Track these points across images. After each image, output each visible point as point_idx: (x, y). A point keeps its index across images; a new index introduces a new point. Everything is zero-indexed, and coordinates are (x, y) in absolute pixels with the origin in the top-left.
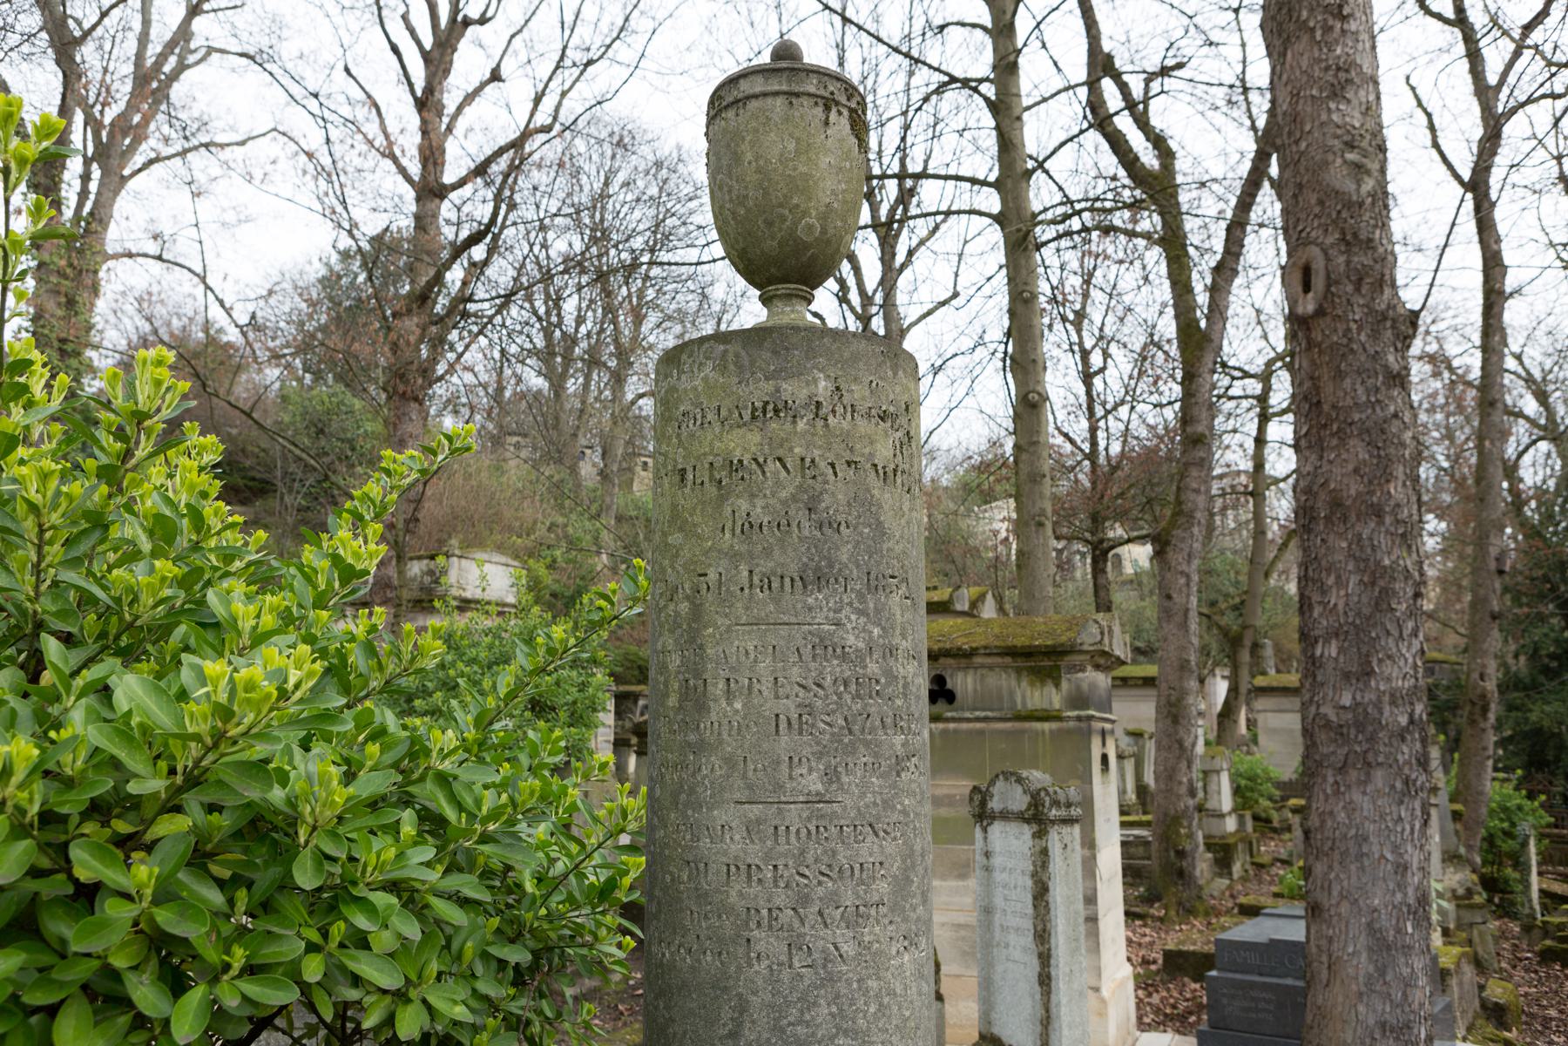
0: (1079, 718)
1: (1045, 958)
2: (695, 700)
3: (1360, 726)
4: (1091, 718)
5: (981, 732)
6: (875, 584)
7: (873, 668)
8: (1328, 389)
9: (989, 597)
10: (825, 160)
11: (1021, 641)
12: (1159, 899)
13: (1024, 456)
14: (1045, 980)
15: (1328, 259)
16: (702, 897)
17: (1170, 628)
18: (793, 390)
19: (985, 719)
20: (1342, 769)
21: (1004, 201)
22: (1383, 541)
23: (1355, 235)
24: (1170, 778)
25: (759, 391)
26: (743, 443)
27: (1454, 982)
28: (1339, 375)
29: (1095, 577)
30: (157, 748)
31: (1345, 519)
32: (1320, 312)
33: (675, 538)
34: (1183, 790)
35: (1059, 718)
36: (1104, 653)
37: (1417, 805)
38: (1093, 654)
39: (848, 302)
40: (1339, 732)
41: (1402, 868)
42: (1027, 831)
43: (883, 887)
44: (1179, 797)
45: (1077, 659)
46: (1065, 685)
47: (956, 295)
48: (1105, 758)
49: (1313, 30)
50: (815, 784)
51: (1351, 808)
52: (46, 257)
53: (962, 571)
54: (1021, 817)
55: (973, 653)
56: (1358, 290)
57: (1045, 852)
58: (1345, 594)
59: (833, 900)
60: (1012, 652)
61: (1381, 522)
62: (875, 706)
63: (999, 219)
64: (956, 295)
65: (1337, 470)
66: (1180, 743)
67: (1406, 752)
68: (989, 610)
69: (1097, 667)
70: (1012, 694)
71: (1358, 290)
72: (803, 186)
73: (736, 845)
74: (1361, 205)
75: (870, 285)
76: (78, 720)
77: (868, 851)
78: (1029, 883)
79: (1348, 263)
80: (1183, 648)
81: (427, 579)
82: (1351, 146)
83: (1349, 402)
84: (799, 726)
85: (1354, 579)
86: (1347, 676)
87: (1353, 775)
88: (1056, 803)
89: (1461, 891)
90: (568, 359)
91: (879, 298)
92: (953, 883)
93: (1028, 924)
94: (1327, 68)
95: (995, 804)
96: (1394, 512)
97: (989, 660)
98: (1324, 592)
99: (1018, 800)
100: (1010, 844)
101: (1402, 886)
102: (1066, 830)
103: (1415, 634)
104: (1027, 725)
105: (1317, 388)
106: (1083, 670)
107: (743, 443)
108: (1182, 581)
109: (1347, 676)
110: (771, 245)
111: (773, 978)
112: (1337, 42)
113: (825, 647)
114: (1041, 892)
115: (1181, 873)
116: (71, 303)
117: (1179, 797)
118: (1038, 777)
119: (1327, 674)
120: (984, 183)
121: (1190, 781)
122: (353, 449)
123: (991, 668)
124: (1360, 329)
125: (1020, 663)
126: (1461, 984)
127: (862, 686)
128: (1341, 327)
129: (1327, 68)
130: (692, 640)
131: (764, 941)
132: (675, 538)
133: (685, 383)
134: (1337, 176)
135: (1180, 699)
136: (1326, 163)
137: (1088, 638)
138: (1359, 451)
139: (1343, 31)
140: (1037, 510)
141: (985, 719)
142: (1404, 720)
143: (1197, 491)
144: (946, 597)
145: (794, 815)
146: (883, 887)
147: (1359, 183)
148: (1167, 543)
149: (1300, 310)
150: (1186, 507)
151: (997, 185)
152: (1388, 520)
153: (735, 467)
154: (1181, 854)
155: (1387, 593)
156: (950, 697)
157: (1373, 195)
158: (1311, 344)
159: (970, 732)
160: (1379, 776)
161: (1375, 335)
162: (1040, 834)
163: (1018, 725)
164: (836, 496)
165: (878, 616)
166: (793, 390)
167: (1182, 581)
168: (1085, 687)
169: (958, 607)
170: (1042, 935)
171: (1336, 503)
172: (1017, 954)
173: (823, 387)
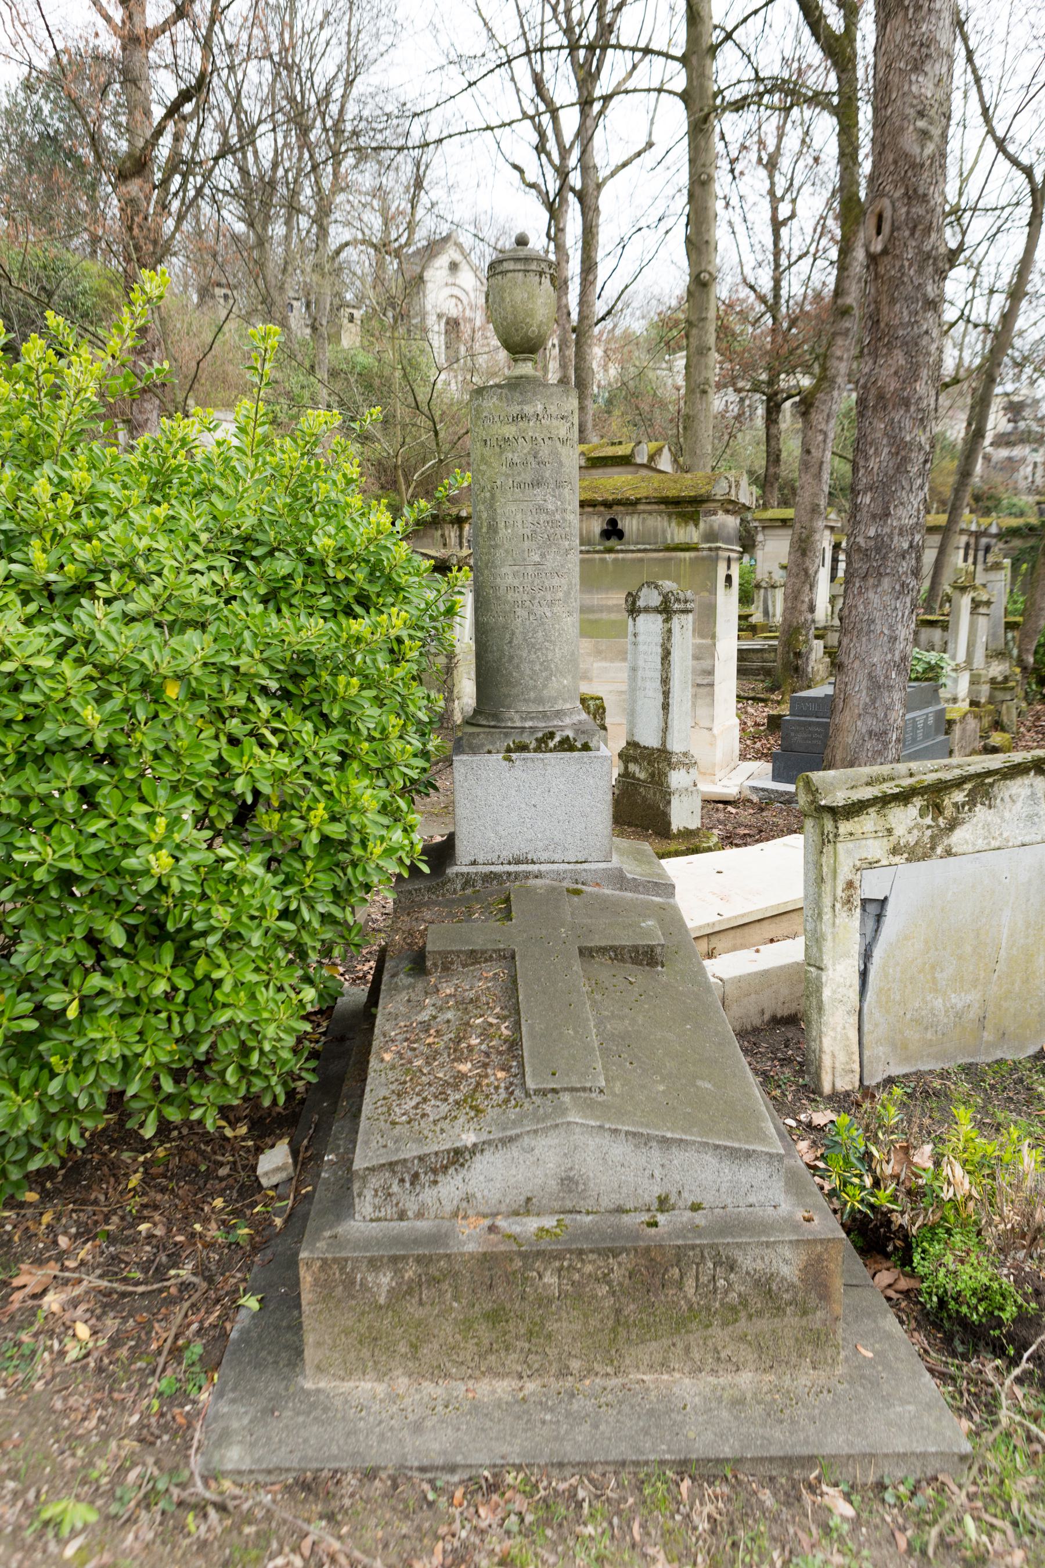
0: (710, 549)
1: (666, 694)
2: (493, 529)
3: (878, 550)
4: (718, 548)
5: (641, 560)
6: (559, 485)
7: (558, 517)
8: (885, 310)
9: (666, 450)
10: (540, 301)
11: (672, 493)
12: (778, 688)
13: (694, 331)
14: (666, 707)
15: (894, 210)
16: (498, 598)
17: (807, 478)
18: (528, 409)
19: (645, 551)
20: (864, 578)
21: (690, 79)
22: (908, 423)
23: (915, 190)
24: (796, 598)
25: (515, 410)
26: (509, 431)
27: (957, 729)
28: (893, 301)
29: (768, 428)
31: (885, 408)
32: (885, 252)
33: (483, 467)
34: (805, 607)
35: (696, 549)
36: (731, 502)
37: (908, 600)
38: (723, 503)
39: (548, 155)
40: (865, 554)
42: (660, 618)
43: (560, 595)
44: (801, 612)
45: (711, 506)
46: (702, 525)
47: (650, 145)
48: (729, 579)
49: (907, 8)
50: (537, 558)
51: (867, 603)
53: (649, 422)
54: (657, 610)
55: (638, 502)
56: (912, 234)
57: (670, 631)
58: (879, 460)
59: (544, 598)
60: (665, 501)
61: (907, 411)
62: (558, 531)
63: (685, 96)
64: (650, 145)
65: (884, 373)
67: (905, 566)
68: (665, 463)
69: (727, 512)
70: (664, 532)
71: (912, 234)
72: (530, 313)
73: (510, 580)
74: (922, 165)
75: (568, 136)
77: (556, 581)
78: (660, 650)
79: (908, 213)
80: (815, 495)
82: (921, 114)
83: (897, 322)
84: (532, 537)
85: (886, 450)
86: (874, 517)
87: (871, 581)
88: (678, 600)
89: (1000, 679)
90: (266, 204)
91: (576, 153)
93: (657, 675)
94: (914, 44)
95: (641, 603)
96: (917, 403)
97: (648, 507)
98: (867, 460)
99: (656, 600)
100: (650, 626)
101: (892, 650)
102: (683, 617)
103: (921, 487)
104: (674, 554)
105: (878, 310)
106: (715, 514)
107: (509, 431)
109: (874, 517)
110: (517, 339)
111: (523, 623)
112: (923, 19)
113: (540, 509)
114: (666, 655)
115: (797, 669)
117: (801, 612)
118: (668, 585)
119: (864, 515)
120: (673, 58)
122: (75, 308)
123: (650, 513)
124: (911, 266)
125: (671, 509)
126: (964, 730)
127: (553, 523)
128: (898, 264)
129: (914, 44)
130: (491, 507)
131: (520, 611)
132: (483, 467)
133: (485, 404)
134: (909, 142)
135: (808, 537)
136: (902, 129)
137: (720, 490)
138: (899, 358)
139: (930, 10)
140: (702, 379)
141: (645, 551)
142: (906, 546)
143: (840, 359)
144: (628, 452)
145: (530, 570)
146: (560, 595)
147: (922, 147)
148: (811, 405)
149: (872, 249)
150: (830, 373)
151: (684, 60)
152: (913, 409)
153: (506, 440)
154: (798, 655)
155: (905, 460)
156: (620, 535)
157: (932, 158)
158: (877, 276)
159: (633, 560)
160: (886, 582)
161: (921, 271)
162: (667, 620)
163: (667, 554)
164: (544, 452)
165: (560, 497)
166: (528, 409)
167: (821, 438)
168: (716, 526)
169: (639, 460)
170: (665, 681)
171: (881, 397)
172: (650, 693)
173: (539, 408)
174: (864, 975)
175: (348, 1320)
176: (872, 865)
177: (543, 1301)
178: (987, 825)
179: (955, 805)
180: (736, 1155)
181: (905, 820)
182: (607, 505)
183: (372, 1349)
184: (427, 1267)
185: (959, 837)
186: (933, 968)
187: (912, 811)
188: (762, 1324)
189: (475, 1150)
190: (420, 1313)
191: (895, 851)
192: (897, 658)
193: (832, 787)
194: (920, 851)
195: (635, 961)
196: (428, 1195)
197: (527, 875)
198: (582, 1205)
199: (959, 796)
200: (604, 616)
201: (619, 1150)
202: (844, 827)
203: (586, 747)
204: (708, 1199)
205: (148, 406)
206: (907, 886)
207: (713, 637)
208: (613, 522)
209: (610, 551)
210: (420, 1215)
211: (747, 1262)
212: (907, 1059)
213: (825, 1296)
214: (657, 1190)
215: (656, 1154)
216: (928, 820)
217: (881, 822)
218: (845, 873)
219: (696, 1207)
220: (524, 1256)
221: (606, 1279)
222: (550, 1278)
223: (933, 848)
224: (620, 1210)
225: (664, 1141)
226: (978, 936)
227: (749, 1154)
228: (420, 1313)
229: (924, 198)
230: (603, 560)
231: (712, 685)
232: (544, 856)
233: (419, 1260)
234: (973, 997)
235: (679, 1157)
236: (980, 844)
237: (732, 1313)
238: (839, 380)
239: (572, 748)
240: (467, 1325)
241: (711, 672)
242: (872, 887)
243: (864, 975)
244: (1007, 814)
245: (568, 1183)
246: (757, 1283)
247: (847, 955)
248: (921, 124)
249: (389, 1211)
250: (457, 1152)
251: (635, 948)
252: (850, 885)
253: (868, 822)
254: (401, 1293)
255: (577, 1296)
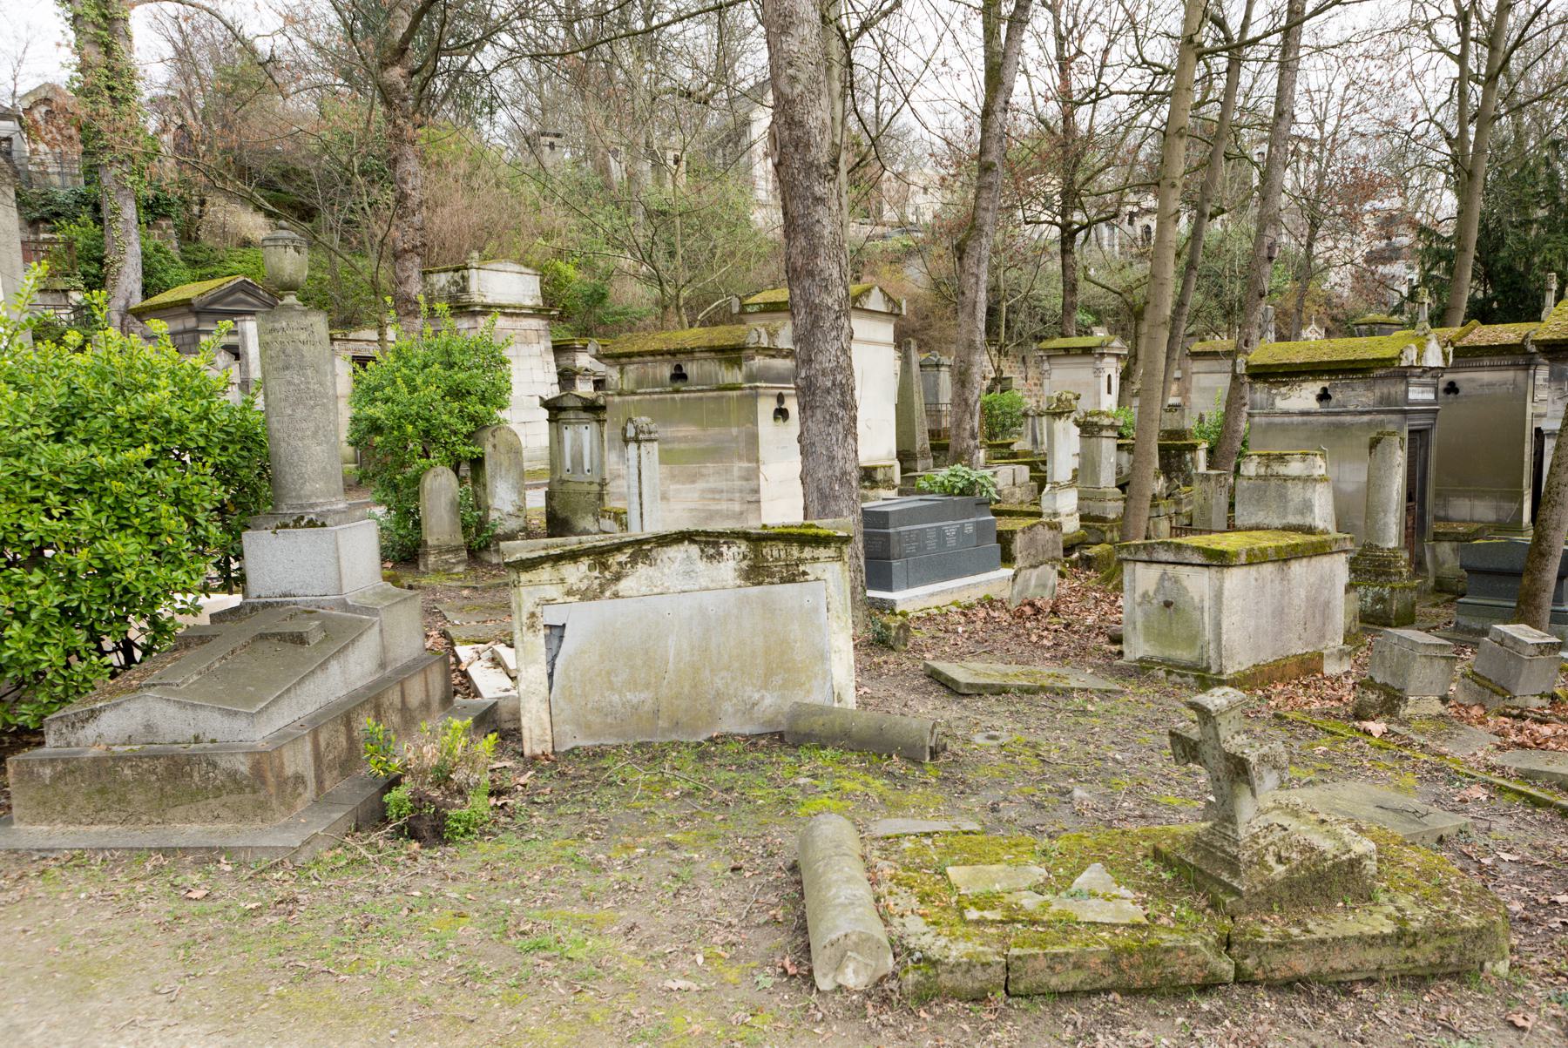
5: (701, 399)
6: (302, 368)
18: (277, 325)
25: (270, 326)
30: (145, 407)
34: (967, 434)
41: (832, 458)
52: (79, 9)
60: (712, 349)
66: (966, 401)
76: (133, 404)
77: (304, 425)
80: (971, 332)
81: (453, 289)
82: (790, 64)
92: (688, 486)
102: (649, 444)
108: (973, 280)
113: (289, 383)
116: (109, 51)
121: (972, 429)
125: (720, 356)
135: (967, 370)
142: (829, 384)
143: (986, 209)
160: (819, 413)
161: (807, 176)
164: (290, 349)
166: (277, 325)
167: (973, 280)
174: (551, 676)
175: (31, 793)
176: (549, 602)
177: (125, 783)
178: (650, 578)
179: (620, 563)
180: (229, 713)
181: (577, 573)
182: (673, 353)
183: (45, 809)
184: (70, 768)
185: (624, 586)
186: (609, 673)
187: (584, 565)
188: (234, 798)
189: (101, 710)
190: (66, 789)
191: (569, 593)
192: (838, 473)
193: (515, 550)
194: (590, 594)
195: (293, 642)
196: (81, 734)
197: (288, 603)
198: (157, 740)
199: (622, 558)
200: (676, 446)
201: (172, 710)
202: (525, 577)
203: (324, 525)
204: (219, 738)
205: (409, 264)
206: (582, 619)
207: (758, 461)
208: (679, 367)
209: (677, 391)
210: (77, 745)
211: (223, 763)
212: (592, 736)
213: (264, 782)
214: (193, 732)
215: (190, 712)
216: (596, 573)
217: (556, 573)
218: (528, 606)
219: (213, 741)
220: (114, 759)
221: (154, 772)
222: (127, 771)
223: (602, 592)
224: (175, 743)
225: (193, 705)
226: (647, 653)
227: (236, 713)
228: (66, 789)
229: (801, 124)
230: (673, 399)
231: (758, 502)
232: (301, 592)
233: (63, 761)
234: (646, 696)
235: (202, 714)
236: (644, 590)
237: (218, 791)
238: (986, 228)
239: (315, 526)
240: (89, 796)
241: (757, 491)
242: (552, 616)
243: (551, 676)
244: (666, 571)
245: (149, 727)
246: (229, 775)
247: (535, 661)
248: (791, 71)
249: (62, 742)
250: (93, 711)
251: (292, 634)
252: (533, 615)
253: (545, 573)
254: (57, 778)
255: (141, 781)
